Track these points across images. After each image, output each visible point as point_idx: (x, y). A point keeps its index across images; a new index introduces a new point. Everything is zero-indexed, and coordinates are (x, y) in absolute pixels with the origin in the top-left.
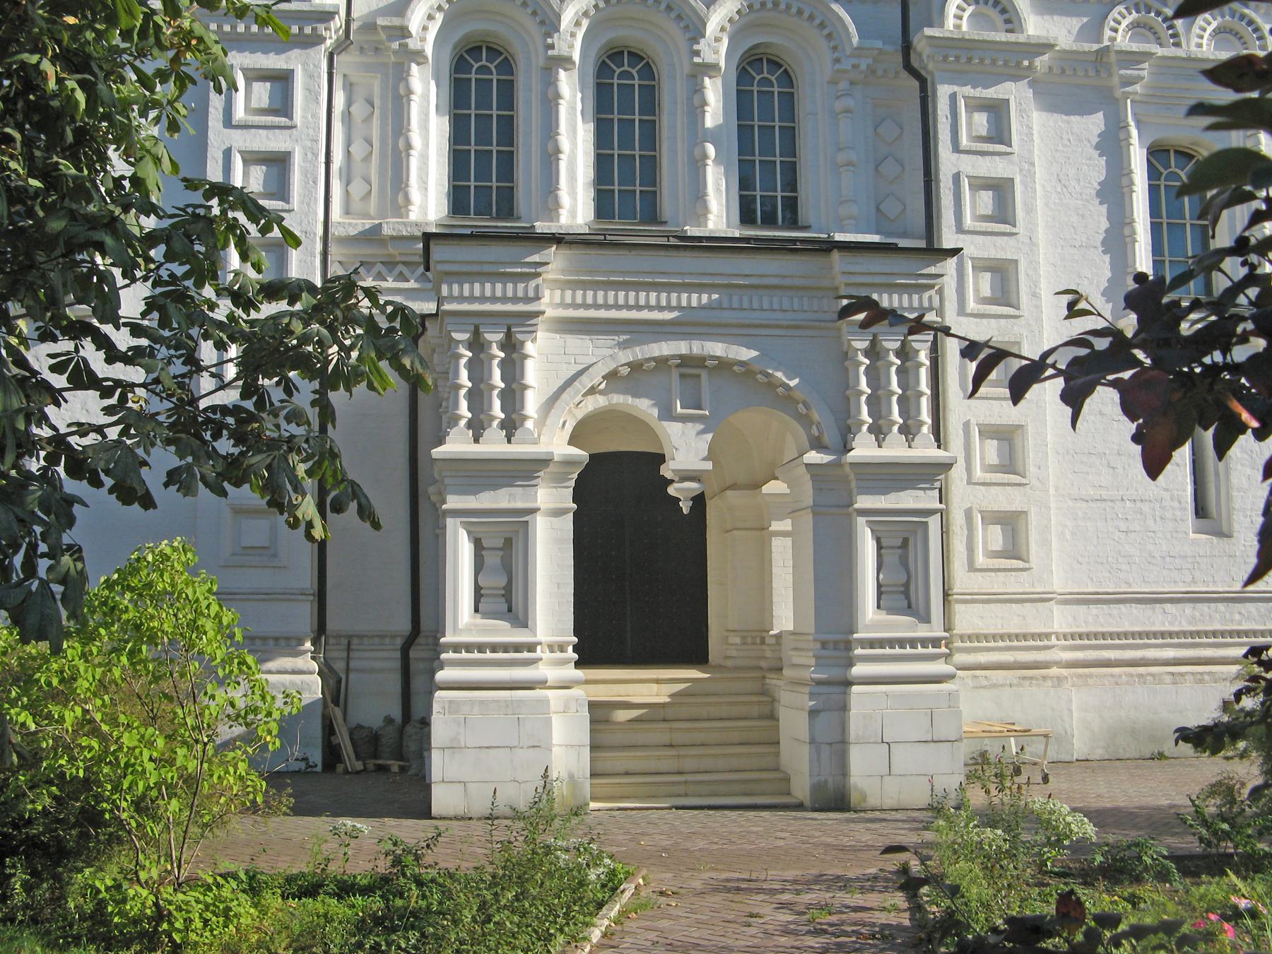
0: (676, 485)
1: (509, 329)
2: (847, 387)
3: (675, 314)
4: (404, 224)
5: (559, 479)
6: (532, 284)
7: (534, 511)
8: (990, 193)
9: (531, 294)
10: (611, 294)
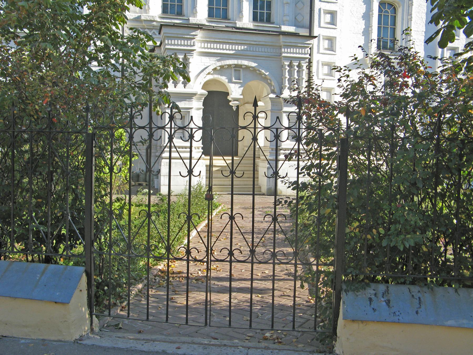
0: (232, 102)
1: (185, 54)
2: (282, 76)
3: (234, 52)
4: (148, 16)
5: (199, 99)
6: (193, 41)
7: (191, 108)
8: (330, 15)
9: (192, 44)
10: (215, 45)
